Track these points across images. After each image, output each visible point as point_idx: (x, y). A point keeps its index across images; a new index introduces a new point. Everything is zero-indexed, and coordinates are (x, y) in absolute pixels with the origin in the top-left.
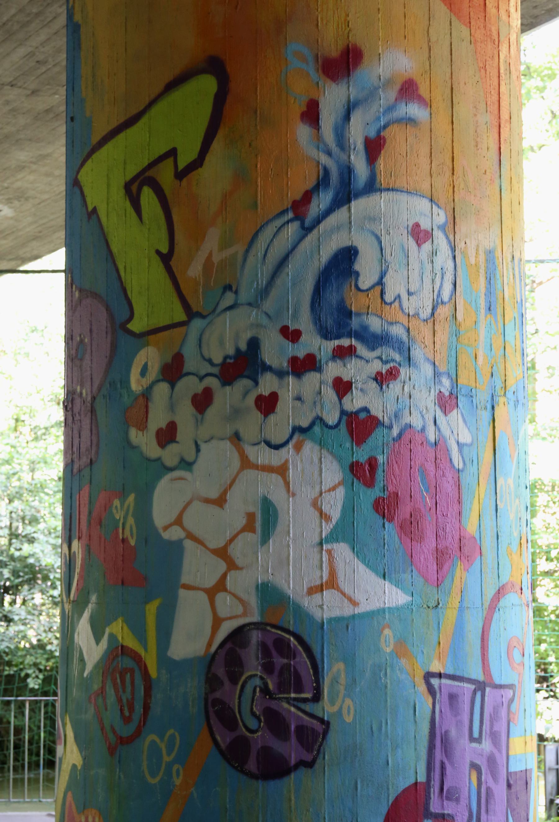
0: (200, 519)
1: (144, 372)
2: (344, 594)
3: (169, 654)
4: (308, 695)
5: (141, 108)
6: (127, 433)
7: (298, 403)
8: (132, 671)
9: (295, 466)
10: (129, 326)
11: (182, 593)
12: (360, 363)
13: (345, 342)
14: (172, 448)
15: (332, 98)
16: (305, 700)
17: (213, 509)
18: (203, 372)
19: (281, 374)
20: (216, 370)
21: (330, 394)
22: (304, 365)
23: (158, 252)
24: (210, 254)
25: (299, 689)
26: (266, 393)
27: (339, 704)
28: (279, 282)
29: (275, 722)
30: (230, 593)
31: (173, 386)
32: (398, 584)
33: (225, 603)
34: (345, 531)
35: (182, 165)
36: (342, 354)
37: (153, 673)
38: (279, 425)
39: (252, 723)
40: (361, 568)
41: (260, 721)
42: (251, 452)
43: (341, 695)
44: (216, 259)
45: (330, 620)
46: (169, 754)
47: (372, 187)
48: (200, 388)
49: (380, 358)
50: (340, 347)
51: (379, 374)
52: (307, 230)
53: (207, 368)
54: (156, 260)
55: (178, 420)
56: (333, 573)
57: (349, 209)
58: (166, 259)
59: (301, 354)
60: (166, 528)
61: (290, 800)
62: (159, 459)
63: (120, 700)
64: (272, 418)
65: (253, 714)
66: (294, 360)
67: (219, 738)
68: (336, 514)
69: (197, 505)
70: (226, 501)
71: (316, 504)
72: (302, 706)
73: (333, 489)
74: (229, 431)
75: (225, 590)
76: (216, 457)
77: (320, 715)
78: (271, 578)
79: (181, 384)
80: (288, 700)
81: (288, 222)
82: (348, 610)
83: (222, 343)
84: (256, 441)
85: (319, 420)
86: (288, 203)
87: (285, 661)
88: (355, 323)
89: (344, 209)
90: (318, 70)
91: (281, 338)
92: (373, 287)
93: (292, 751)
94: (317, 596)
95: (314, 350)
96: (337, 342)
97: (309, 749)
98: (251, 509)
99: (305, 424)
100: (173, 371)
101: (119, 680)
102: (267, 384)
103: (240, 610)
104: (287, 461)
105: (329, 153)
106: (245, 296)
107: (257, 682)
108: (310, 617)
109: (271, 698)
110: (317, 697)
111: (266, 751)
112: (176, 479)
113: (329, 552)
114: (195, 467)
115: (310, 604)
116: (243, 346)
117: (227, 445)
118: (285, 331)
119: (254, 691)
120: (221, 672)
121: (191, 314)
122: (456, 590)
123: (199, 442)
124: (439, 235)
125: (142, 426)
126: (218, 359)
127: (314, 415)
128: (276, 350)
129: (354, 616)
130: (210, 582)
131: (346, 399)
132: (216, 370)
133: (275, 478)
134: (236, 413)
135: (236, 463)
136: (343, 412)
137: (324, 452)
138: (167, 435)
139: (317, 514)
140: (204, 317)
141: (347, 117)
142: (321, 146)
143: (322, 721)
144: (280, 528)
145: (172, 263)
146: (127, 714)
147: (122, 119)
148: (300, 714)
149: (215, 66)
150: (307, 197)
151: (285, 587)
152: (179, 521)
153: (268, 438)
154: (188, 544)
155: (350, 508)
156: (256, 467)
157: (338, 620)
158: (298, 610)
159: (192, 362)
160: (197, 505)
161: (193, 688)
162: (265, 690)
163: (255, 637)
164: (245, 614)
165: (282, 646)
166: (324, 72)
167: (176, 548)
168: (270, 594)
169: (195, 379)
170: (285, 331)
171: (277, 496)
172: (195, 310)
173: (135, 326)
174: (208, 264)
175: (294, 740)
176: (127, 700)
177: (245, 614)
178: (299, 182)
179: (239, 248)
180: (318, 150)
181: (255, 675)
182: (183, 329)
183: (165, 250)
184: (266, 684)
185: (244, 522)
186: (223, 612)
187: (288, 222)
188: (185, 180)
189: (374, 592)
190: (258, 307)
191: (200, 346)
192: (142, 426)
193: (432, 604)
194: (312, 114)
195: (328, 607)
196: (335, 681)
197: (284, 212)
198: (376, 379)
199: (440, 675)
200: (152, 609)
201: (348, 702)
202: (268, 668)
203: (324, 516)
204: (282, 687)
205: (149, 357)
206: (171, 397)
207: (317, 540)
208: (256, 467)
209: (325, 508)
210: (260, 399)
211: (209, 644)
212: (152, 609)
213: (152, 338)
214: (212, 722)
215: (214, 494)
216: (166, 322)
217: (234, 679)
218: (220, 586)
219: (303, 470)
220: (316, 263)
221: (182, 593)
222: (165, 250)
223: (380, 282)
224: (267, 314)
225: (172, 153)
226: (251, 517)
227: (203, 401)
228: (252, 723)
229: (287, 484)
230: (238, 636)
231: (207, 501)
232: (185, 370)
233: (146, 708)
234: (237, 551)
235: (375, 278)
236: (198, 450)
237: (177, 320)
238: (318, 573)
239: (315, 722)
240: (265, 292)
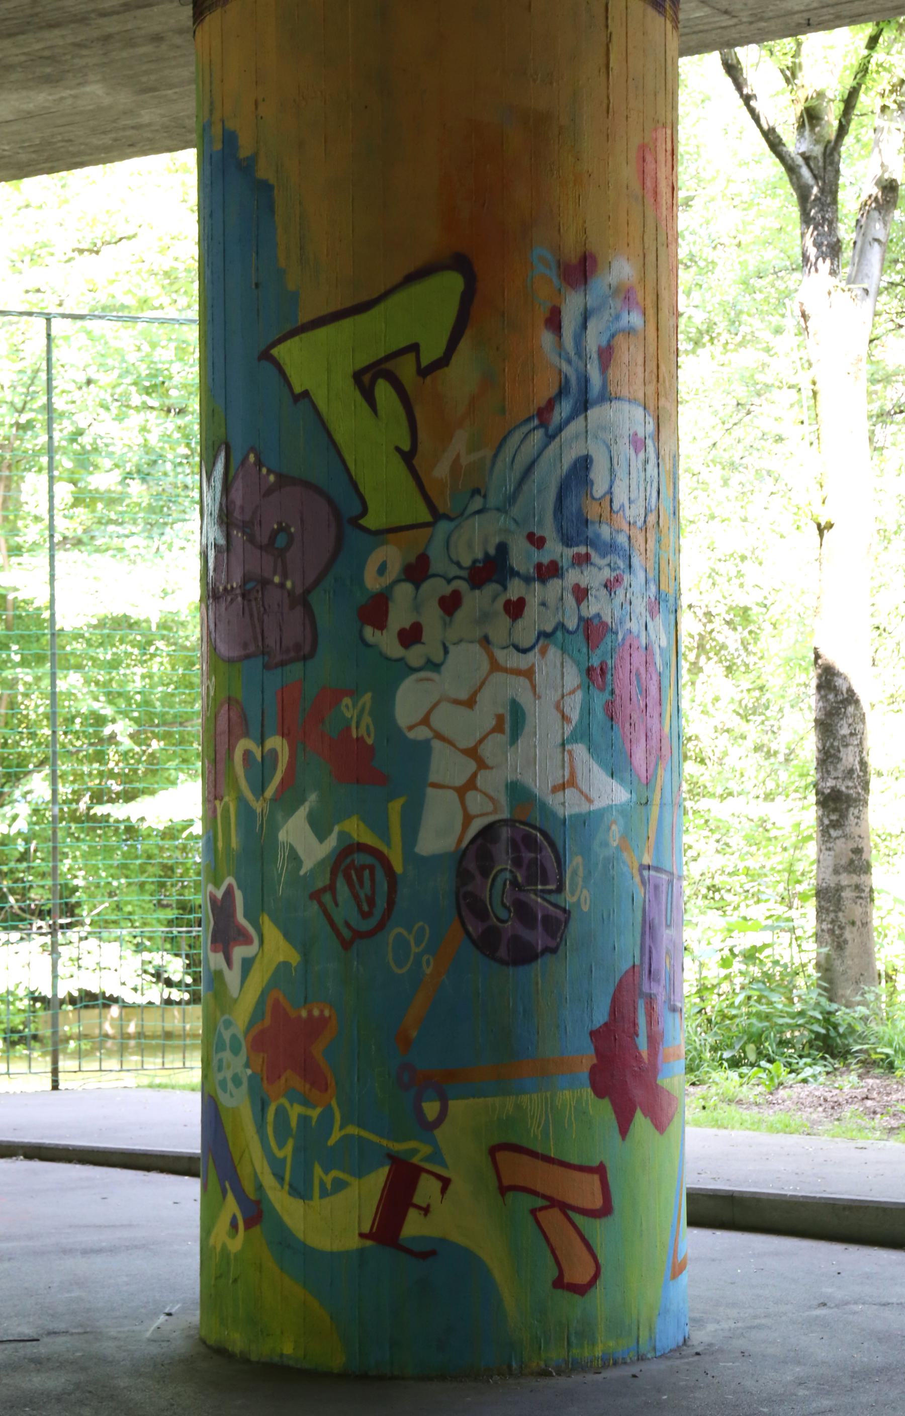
0: (448, 720)
1: (382, 570)
2: (582, 793)
3: (417, 850)
4: (552, 887)
5: (375, 295)
6: (361, 632)
7: (543, 609)
8: (372, 868)
9: (541, 670)
10: (362, 522)
11: (430, 791)
12: (594, 570)
13: (582, 550)
14: (417, 649)
15: (572, 306)
16: (550, 892)
17: (463, 710)
18: (451, 575)
19: (528, 580)
20: (464, 574)
21: (570, 599)
22: (549, 572)
23: (398, 449)
24: (458, 456)
25: (544, 883)
26: (514, 598)
27: (578, 895)
28: (525, 488)
29: (524, 912)
30: (481, 791)
31: (417, 587)
32: (622, 781)
33: (475, 802)
34: (583, 734)
35: (425, 362)
36: (582, 560)
37: (398, 868)
38: (526, 629)
39: (503, 914)
40: (595, 768)
41: (510, 911)
42: (501, 656)
43: (579, 887)
44: (464, 461)
45: (571, 816)
46: (418, 944)
47: (606, 397)
48: (447, 590)
49: (609, 565)
50: (578, 554)
51: (609, 580)
52: (550, 438)
53: (454, 571)
54: (397, 459)
55: (424, 621)
56: (573, 774)
57: (586, 417)
58: (408, 457)
59: (545, 561)
60: (411, 728)
61: (537, 983)
62: (401, 659)
63: (356, 897)
64: (520, 623)
65: (503, 905)
66: (539, 566)
67: (470, 929)
68: (575, 716)
69: (445, 707)
70: (475, 702)
71: (559, 707)
72: (548, 897)
73: (573, 692)
74: (478, 634)
75: (475, 788)
76: (465, 660)
77: (563, 905)
78: (519, 776)
79: (426, 586)
80: (535, 892)
81: (534, 429)
82: (585, 808)
83: (470, 546)
84: (505, 644)
85: (561, 626)
86: (533, 410)
87: (533, 855)
88: (590, 532)
89: (581, 418)
90: (559, 276)
91: (528, 545)
92: (604, 495)
93: (539, 938)
94: (560, 794)
95: (556, 557)
96: (576, 550)
97: (553, 937)
98: (501, 711)
99: (549, 629)
100: (417, 571)
101: (354, 877)
102: (515, 589)
103: (490, 807)
104: (533, 665)
105: (569, 362)
106: (493, 500)
107: (508, 875)
108: (554, 815)
109: (520, 890)
110: (560, 889)
111: (516, 939)
112: (421, 680)
113: (570, 752)
114: (443, 668)
115: (553, 801)
116: (492, 551)
117: (476, 648)
118: (531, 537)
119: (505, 884)
120: (472, 866)
121: (437, 515)
122: (658, 789)
123: (447, 644)
124: (649, 442)
125: (380, 624)
126: (467, 562)
127: (557, 620)
128: (522, 557)
129: (590, 812)
130: (460, 781)
131: (584, 605)
132: (464, 574)
133: (523, 681)
134: (485, 617)
135: (486, 666)
136: (581, 618)
137: (566, 657)
138: (411, 636)
139: (559, 716)
140: (450, 519)
141: (584, 326)
142: (563, 353)
143: (564, 910)
144: (527, 729)
145: (415, 462)
146: (366, 908)
147: (348, 304)
148: (546, 904)
149: (461, 263)
150: (551, 405)
151: (533, 785)
152: (425, 721)
153: (516, 642)
154: (437, 744)
155: (587, 711)
156: (506, 670)
157: (578, 816)
158: (543, 806)
159: (438, 564)
160: (445, 707)
161: (444, 882)
162: (515, 883)
163: (505, 833)
164: (495, 811)
165: (530, 842)
166: (565, 279)
167: (424, 747)
168: (519, 793)
169: (444, 582)
170: (531, 537)
171: (525, 699)
172: (441, 511)
173: (369, 522)
174: (456, 465)
175: (540, 928)
176: (366, 896)
177: (495, 811)
178: (545, 390)
179: (488, 453)
180: (560, 356)
181: (506, 869)
182: (428, 530)
183: (406, 447)
184: (515, 877)
185: (494, 723)
186: (473, 809)
187: (534, 429)
188: (429, 379)
189: (608, 793)
190: (506, 512)
191: (448, 549)
192: (380, 624)
193: (644, 801)
194: (554, 322)
195: (569, 805)
196: (575, 873)
197: (529, 419)
198: (606, 586)
199: (649, 867)
200: (395, 808)
201: (585, 892)
202: (517, 862)
203: (565, 718)
204: (531, 879)
205: (390, 557)
206: (415, 598)
207: (560, 741)
208: (506, 670)
209: (567, 710)
210: (508, 604)
211: (460, 840)
212: (395, 808)
213: (391, 536)
214: (463, 914)
215: (464, 695)
216: (408, 521)
217: (485, 873)
218: (471, 784)
219: (547, 674)
220: (559, 471)
221: (430, 791)
222: (406, 447)
223: (610, 492)
224: (515, 521)
225: (414, 348)
226: (500, 718)
227: (450, 604)
228: (503, 914)
229: (534, 687)
230: (488, 832)
231: (457, 702)
232: (432, 570)
233: (391, 903)
234: (487, 751)
235: (605, 487)
236: (446, 651)
237: (421, 520)
238: (561, 773)
239: (558, 911)
240: (512, 499)
